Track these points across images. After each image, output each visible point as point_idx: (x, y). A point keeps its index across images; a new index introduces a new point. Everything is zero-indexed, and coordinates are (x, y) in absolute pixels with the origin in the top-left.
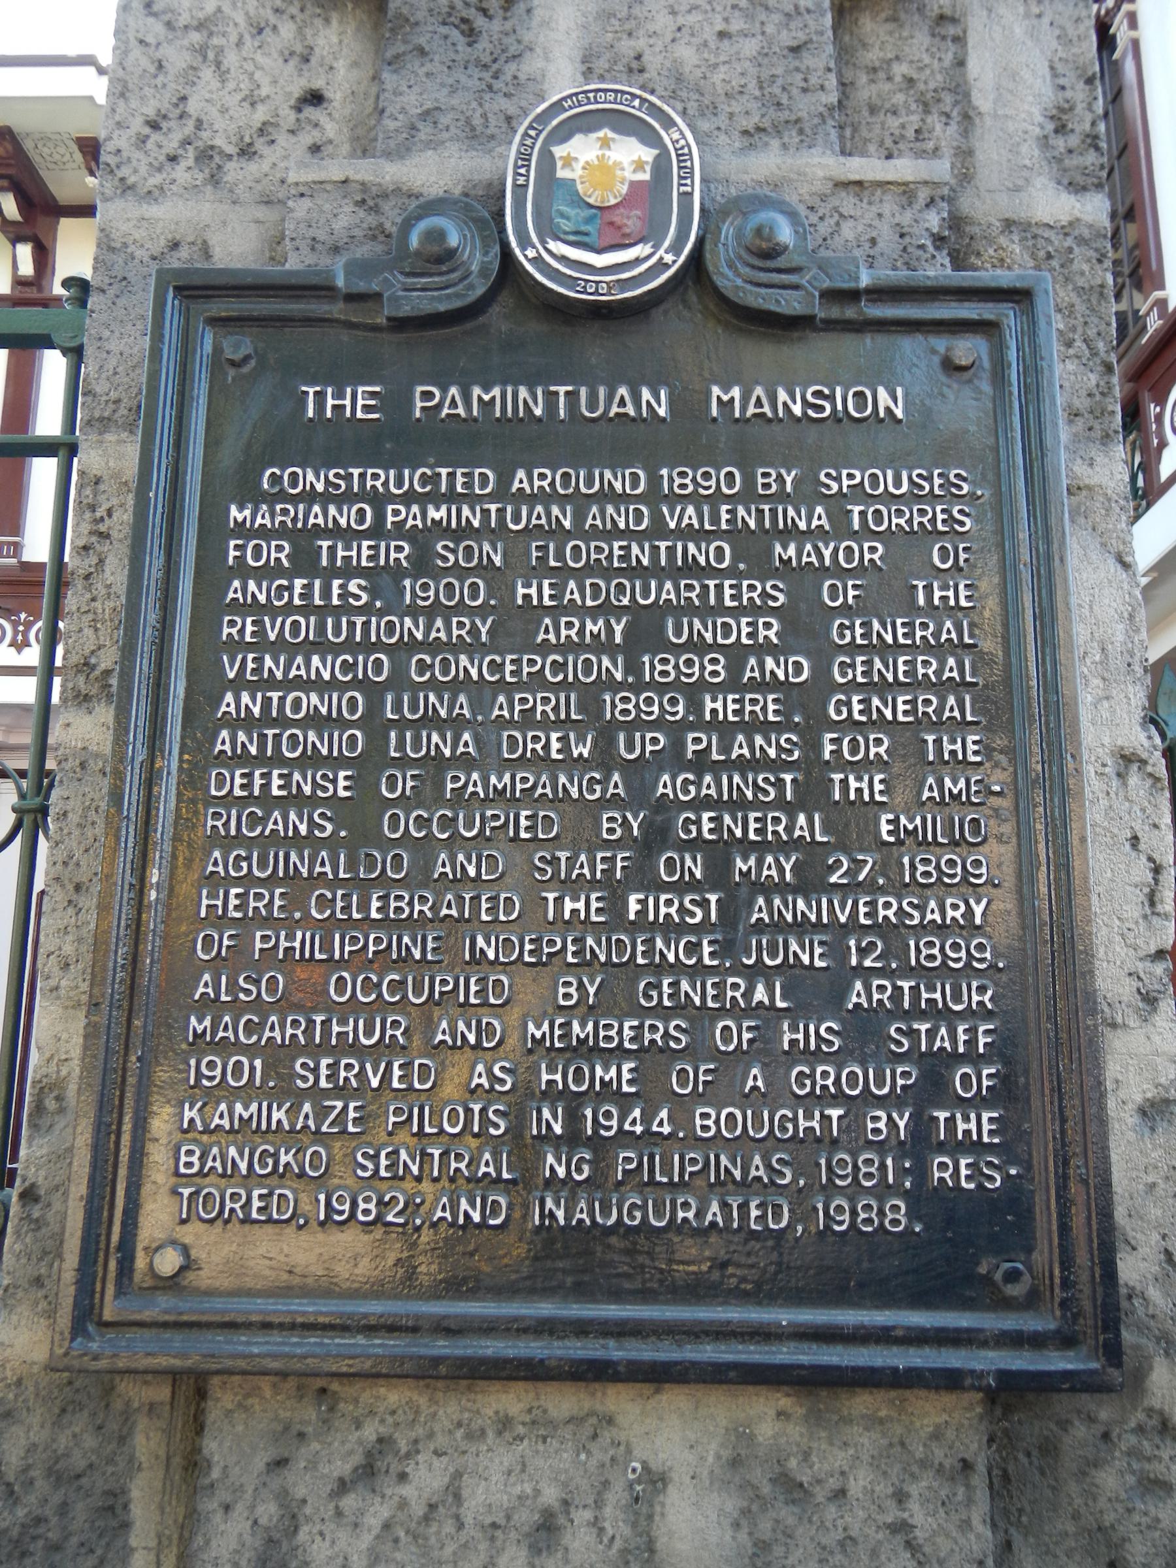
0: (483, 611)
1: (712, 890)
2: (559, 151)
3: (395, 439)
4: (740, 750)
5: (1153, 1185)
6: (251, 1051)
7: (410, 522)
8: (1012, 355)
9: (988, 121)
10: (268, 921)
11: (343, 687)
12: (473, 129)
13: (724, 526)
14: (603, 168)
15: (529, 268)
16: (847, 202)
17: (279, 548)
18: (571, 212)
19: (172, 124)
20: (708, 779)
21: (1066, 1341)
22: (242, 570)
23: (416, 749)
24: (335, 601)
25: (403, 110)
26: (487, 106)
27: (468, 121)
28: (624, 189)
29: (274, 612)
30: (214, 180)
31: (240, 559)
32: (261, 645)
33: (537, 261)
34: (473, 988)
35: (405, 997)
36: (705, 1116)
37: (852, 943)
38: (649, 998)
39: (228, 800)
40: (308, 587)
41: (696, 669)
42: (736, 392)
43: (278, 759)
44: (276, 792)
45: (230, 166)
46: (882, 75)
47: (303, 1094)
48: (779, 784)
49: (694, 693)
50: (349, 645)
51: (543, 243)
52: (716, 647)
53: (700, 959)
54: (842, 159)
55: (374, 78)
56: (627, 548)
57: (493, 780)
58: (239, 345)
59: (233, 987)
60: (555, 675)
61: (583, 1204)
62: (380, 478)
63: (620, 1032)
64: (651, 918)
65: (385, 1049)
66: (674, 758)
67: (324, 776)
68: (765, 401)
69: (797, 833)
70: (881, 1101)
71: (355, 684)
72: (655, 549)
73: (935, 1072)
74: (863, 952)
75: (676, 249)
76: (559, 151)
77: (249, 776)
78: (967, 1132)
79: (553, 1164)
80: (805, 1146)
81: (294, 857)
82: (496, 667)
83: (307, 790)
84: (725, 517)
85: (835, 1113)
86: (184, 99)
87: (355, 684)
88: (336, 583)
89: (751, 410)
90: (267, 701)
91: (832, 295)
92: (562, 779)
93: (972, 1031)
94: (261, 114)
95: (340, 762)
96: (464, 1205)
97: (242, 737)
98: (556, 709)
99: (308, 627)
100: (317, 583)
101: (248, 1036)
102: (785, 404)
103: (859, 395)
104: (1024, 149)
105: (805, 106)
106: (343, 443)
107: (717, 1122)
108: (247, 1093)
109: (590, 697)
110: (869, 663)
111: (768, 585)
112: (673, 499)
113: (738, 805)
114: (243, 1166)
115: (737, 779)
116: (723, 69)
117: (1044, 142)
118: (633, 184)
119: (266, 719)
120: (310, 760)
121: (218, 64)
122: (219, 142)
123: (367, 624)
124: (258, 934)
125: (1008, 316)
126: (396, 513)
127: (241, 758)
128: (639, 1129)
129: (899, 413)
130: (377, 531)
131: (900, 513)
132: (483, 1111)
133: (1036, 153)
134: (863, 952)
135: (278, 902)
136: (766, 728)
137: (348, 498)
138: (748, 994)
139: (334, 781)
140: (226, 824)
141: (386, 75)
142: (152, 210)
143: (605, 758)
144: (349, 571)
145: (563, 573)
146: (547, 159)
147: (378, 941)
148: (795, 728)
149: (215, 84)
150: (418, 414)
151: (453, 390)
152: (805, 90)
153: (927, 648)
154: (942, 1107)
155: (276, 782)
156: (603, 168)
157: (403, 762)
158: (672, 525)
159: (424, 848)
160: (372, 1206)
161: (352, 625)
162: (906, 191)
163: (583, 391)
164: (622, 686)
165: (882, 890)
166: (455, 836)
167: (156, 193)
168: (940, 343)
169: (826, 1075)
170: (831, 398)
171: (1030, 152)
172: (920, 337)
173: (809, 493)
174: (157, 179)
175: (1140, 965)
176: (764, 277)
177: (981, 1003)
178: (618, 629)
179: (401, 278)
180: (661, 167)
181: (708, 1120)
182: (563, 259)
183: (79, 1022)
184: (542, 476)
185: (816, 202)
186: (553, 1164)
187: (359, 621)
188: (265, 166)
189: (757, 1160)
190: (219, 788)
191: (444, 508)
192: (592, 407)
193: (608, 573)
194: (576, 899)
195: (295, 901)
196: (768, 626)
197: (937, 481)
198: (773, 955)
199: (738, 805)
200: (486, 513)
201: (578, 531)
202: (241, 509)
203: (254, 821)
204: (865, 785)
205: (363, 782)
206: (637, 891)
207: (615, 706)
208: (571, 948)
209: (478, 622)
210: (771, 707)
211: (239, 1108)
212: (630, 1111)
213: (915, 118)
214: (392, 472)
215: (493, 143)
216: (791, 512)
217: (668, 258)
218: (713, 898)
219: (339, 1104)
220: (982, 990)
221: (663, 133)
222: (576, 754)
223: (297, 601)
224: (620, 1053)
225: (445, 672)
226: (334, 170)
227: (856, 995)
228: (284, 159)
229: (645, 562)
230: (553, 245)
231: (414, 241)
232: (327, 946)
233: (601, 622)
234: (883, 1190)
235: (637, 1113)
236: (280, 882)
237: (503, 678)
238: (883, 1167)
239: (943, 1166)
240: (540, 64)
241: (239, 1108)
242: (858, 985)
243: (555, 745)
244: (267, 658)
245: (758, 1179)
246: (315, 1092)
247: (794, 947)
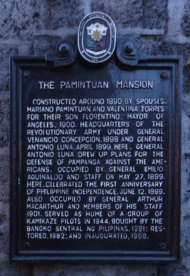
0: (74, 128)
1: (115, 181)
2: (88, 28)
3: (57, 93)
4: (121, 155)
5: (185, 230)
6: (38, 210)
7: (61, 111)
8: (174, 74)
9: (171, 20)
10: (39, 188)
11: (50, 144)
12: (70, 23)
13: (119, 111)
14: (97, 33)
15: (83, 55)
16: (143, 40)
17: (37, 116)
18: (91, 42)
19: (9, 21)
20: (115, 160)
21: (170, 256)
22: (30, 121)
23: (63, 155)
24: (48, 127)
25: (56, 18)
26: (72, 17)
27: (69, 20)
28: (101, 37)
29: (37, 129)
30: (18, 34)
31: (30, 118)
32: (35, 136)
33: (84, 54)
34: (75, 199)
35: (63, 201)
36: (114, 220)
37: (139, 190)
38: (104, 200)
39: (31, 166)
40: (42, 124)
41: (113, 139)
43: (39, 158)
44: (39, 164)
45: (21, 31)
46: (150, 9)
47: (47, 218)
48: (127, 161)
49: (113, 144)
50: (50, 136)
51: (85, 50)
52: (117, 135)
53: (113, 193)
54: (143, 29)
55: (49, 10)
56: (101, 116)
57: (77, 161)
58: (27, 74)
59: (34, 199)
60: (88, 141)
61: (93, 235)
62: (54, 101)
63: (99, 206)
64: (105, 186)
65: (59, 210)
66: (108, 157)
67: (47, 161)
69: (130, 171)
70: (143, 217)
71: (52, 143)
72: (106, 116)
73: (152, 213)
74: (141, 192)
75: (111, 51)
76: (88, 28)
77: (34, 161)
78: (157, 222)
79: (89, 229)
80: (130, 226)
81: (43, 176)
82: (77, 140)
83: (44, 163)
84: (119, 109)
85: (135, 219)
86: (11, 15)
87: (52, 143)
88: (48, 123)
89: (124, 86)
90: (36, 147)
91: (140, 61)
92: (89, 161)
93: (159, 205)
94: (26, 19)
95: (49, 158)
96: (74, 235)
97: (32, 153)
98: (88, 147)
99: (43, 132)
100: (44, 123)
101: (37, 208)
102: (130, 85)
103: (144, 83)
104: (178, 26)
105: (137, 16)
106: (47, 94)
107: (116, 221)
108: (37, 218)
109: (94, 145)
110: (144, 138)
111: (126, 123)
112: (109, 105)
113: (120, 165)
114: (37, 230)
115: (120, 160)
116: (120, 8)
117: (182, 25)
118: (103, 36)
119: (36, 150)
120: (45, 158)
121: (17, 7)
122: (18, 26)
123: (53, 131)
124: (37, 190)
125: (173, 65)
126: (58, 108)
127: (33, 158)
128: (103, 222)
129: (152, 87)
130: (54, 112)
131: (151, 108)
132: (77, 220)
133: (180, 27)
134: (141, 192)
135: (40, 184)
136: (125, 151)
137: (49, 106)
138: (121, 200)
139: (49, 162)
140: (31, 170)
141: (52, 10)
142: (7, 42)
143: (96, 157)
144: (50, 120)
145: (89, 120)
146: (86, 30)
147: (58, 191)
148: (130, 151)
149: (17, 11)
151: (68, 83)
152: (136, 13)
153: (154, 135)
154: (153, 218)
155: (39, 162)
156: (97, 33)
157: (61, 158)
158: (109, 111)
159: (65, 174)
160: (59, 236)
161: (51, 131)
162: (154, 37)
163: (92, 83)
164: (100, 143)
165: (145, 181)
166: (71, 172)
167: (7, 38)
168: (160, 72)
169: (134, 213)
170: (139, 84)
171: (179, 27)
172: (156, 71)
173: (135, 103)
174: (6, 35)
175: (186, 193)
176: (127, 57)
177: (160, 200)
178: (99, 132)
179: (58, 58)
180: (108, 31)
181: (114, 221)
182: (89, 53)
183: (8, 206)
184: (85, 101)
185: (137, 39)
186: (89, 229)
187: (52, 130)
188: (28, 32)
189: (122, 227)
190: (29, 163)
191: (67, 107)
193: (97, 120)
194: (92, 183)
195: (43, 184)
196: (126, 131)
197: (158, 101)
198: (125, 192)
199: (120, 165)
200: (75, 108)
201: (92, 112)
202: (29, 108)
203: (35, 169)
204: (142, 161)
205: (54, 162)
206: (102, 181)
207: (99, 147)
208: (91, 192)
209: (74, 130)
210: (126, 147)
211: (36, 220)
212: (101, 219)
213: (156, 19)
214: (57, 100)
216: (131, 107)
217: (110, 53)
218: (115, 182)
219: (53, 219)
220: (160, 198)
221: (109, 24)
222: (91, 156)
223: (41, 127)
224: (99, 210)
225: (68, 140)
226: (43, 32)
227: (139, 199)
228: (32, 29)
229: (104, 118)
230: (87, 50)
231: (60, 49)
232: (49, 192)
233: (96, 130)
234: (142, 232)
235: (102, 220)
236: (41, 181)
237: (78, 141)
238: (143, 228)
239: (152, 228)
240: (83, 7)
241: (36, 220)
242: (140, 197)
243: (88, 154)
244: (36, 138)
245: (122, 230)
246: (49, 217)
247: (129, 191)
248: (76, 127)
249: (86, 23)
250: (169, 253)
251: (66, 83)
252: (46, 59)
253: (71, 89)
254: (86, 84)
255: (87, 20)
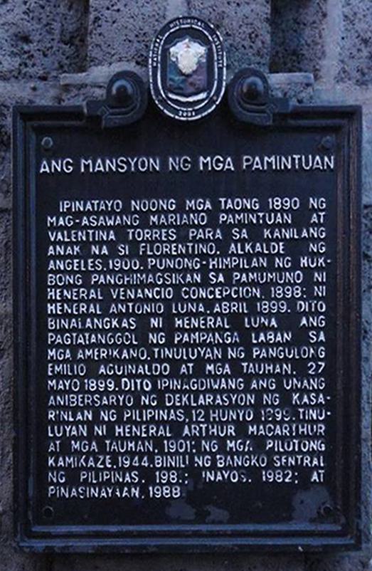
40: (79, 263)
42: (209, 159)
68: (101, 165)
74: (197, 416)
82: (212, 293)
150: (244, 167)
158: (52, 239)
192: (307, 165)
215: (288, 82)
231: (114, 91)
248: (142, 268)
249: (203, 31)
250: (340, 528)
251: (254, 159)
252: (85, 110)
253: (263, 171)
254: (293, 159)
255: (208, 31)
